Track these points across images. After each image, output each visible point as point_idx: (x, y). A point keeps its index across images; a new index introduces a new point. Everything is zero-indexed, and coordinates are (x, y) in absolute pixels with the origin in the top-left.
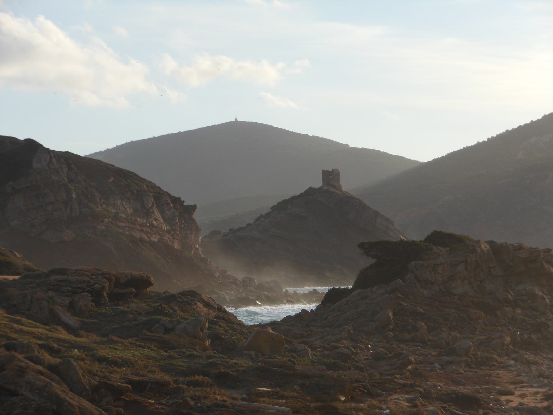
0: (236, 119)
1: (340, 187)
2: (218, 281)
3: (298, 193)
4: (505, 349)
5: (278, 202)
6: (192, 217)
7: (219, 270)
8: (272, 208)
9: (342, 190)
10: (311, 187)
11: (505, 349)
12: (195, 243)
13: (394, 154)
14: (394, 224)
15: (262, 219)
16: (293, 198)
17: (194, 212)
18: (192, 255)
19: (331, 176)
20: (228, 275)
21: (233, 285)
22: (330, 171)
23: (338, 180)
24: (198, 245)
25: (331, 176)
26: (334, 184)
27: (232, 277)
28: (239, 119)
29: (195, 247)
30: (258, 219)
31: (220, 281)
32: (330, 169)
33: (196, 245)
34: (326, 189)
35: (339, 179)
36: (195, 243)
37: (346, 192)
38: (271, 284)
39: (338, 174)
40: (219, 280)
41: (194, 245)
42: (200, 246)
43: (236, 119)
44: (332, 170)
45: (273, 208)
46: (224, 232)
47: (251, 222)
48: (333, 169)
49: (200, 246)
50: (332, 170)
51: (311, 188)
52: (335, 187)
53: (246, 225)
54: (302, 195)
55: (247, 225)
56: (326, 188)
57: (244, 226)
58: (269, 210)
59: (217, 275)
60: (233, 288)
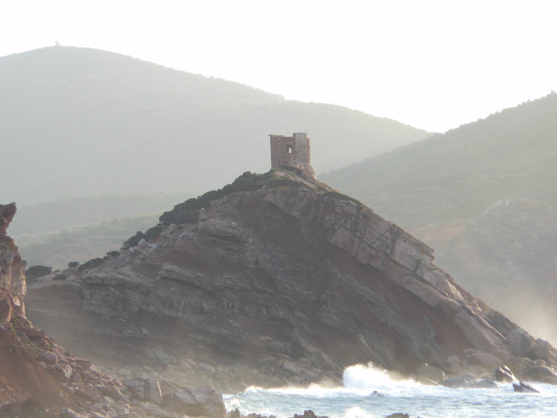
0: (57, 43)
1: (311, 173)
2: (72, 388)
3: (220, 186)
4: (63, 352)
5: (176, 204)
6: (5, 233)
7: (73, 361)
8: (161, 218)
9: (314, 180)
10: (249, 173)
11: (63, 352)
12: (13, 294)
13: (376, 115)
14: (433, 255)
15: (142, 242)
16: (211, 196)
17: (10, 221)
18: (9, 325)
19: (290, 149)
20: (94, 372)
21: (107, 398)
22: (289, 139)
23: (306, 159)
24: (20, 300)
25: (290, 149)
26: (298, 166)
27: (103, 377)
28: (62, 44)
29: (12, 303)
30: (133, 242)
31: (77, 388)
32: (289, 134)
33: (14, 300)
34: (282, 177)
35: (309, 155)
36: (13, 294)
37: (322, 184)
38: (197, 396)
39: (306, 146)
40: (74, 384)
41: (11, 300)
42: (23, 303)
43: (57, 43)
44: (292, 136)
45: (166, 218)
46: (58, 271)
47: (117, 248)
48: (294, 134)
49: (23, 303)
50: (292, 136)
51: (247, 175)
52: (299, 173)
53: (106, 255)
54: (228, 190)
55: (108, 254)
56: (280, 174)
57: (101, 256)
58: (154, 222)
59: (68, 372)
60: (109, 405)
